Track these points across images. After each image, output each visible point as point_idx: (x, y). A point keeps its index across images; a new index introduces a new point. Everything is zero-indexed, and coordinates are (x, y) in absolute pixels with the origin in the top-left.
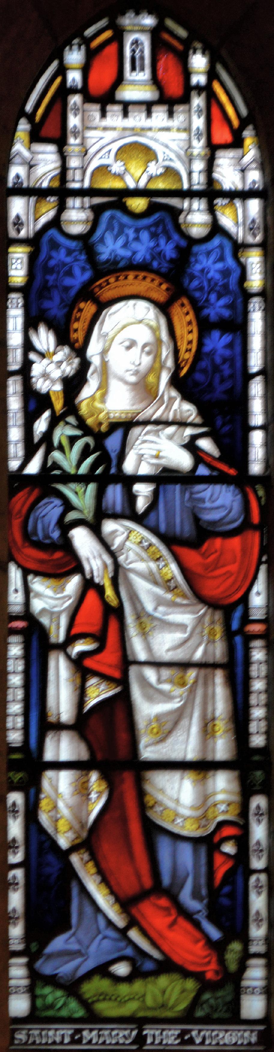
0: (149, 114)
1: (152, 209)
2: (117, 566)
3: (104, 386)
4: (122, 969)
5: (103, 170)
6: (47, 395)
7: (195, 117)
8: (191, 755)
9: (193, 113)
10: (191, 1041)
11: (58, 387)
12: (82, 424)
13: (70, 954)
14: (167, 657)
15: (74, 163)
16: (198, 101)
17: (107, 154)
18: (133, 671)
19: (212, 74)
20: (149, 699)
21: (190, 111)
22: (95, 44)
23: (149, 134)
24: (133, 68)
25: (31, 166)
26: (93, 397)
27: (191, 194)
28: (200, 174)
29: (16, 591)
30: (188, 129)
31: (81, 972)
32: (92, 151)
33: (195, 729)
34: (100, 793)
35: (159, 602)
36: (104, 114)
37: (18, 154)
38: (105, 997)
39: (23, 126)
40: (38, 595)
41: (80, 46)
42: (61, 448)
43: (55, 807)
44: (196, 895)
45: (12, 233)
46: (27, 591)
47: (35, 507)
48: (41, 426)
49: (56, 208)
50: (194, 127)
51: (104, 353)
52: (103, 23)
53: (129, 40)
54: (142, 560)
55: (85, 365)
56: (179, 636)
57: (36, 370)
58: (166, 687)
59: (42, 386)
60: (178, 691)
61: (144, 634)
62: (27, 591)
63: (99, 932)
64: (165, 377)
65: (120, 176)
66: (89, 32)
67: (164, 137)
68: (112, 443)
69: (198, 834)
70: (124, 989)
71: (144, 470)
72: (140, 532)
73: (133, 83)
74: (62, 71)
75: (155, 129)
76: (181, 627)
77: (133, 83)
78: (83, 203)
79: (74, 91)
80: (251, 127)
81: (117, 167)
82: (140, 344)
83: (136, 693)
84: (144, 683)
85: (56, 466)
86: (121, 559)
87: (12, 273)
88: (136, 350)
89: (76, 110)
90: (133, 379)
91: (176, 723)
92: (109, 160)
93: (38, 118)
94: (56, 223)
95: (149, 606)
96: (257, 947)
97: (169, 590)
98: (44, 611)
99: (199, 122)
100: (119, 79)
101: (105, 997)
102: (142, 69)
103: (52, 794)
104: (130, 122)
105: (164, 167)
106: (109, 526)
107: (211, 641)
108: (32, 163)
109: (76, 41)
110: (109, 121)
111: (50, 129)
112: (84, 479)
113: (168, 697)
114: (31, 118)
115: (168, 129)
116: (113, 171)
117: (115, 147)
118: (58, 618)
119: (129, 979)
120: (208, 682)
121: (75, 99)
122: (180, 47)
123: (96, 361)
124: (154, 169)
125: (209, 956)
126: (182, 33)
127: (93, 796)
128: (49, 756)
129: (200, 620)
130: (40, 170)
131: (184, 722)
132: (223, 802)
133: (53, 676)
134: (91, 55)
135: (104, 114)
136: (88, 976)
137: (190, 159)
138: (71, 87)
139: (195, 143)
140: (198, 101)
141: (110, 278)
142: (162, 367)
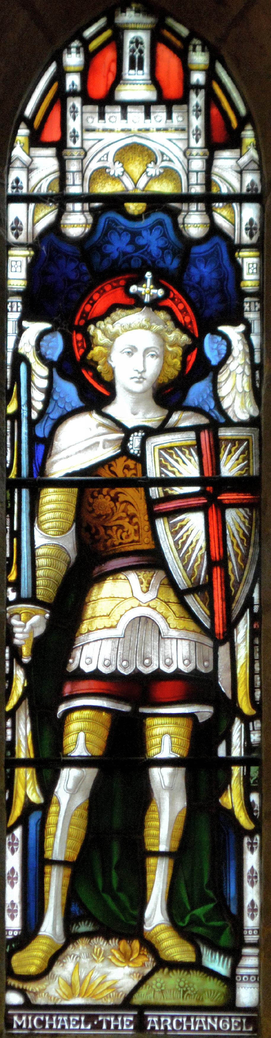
5: (102, 172)
7: (193, 118)
8: (37, 544)
9: (191, 114)
15: (73, 166)
16: (197, 100)
17: (106, 156)
19: (211, 74)
21: (188, 111)
22: (93, 45)
23: (148, 135)
24: (132, 67)
25: (29, 170)
28: (49, 412)
32: (90, 154)
36: (102, 116)
37: (18, 159)
39: (23, 132)
41: (78, 49)
45: (11, 237)
49: (57, 210)
50: (193, 127)
52: (102, 22)
53: (130, 36)
65: (118, 179)
66: (88, 33)
73: (133, 82)
74: (60, 75)
75: (153, 131)
78: (83, 207)
80: (249, 127)
81: (117, 169)
87: (10, 275)
88: (138, 355)
93: (37, 123)
96: (251, 938)
99: (197, 122)
100: (118, 79)
102: (141, 68)
105: (162, 167)
108: (31, 167)
109: (76, 44)
114: (29, 123)
115: (166, 130)
116: (112, 173)
121: (76, 102)
126: (184, 31)
133: (32, 794)
134: (89, 57)
135: (102, 116)
138: (70, 90)
139: (193, 143)
140: (197, 100)
141: (104, 286)
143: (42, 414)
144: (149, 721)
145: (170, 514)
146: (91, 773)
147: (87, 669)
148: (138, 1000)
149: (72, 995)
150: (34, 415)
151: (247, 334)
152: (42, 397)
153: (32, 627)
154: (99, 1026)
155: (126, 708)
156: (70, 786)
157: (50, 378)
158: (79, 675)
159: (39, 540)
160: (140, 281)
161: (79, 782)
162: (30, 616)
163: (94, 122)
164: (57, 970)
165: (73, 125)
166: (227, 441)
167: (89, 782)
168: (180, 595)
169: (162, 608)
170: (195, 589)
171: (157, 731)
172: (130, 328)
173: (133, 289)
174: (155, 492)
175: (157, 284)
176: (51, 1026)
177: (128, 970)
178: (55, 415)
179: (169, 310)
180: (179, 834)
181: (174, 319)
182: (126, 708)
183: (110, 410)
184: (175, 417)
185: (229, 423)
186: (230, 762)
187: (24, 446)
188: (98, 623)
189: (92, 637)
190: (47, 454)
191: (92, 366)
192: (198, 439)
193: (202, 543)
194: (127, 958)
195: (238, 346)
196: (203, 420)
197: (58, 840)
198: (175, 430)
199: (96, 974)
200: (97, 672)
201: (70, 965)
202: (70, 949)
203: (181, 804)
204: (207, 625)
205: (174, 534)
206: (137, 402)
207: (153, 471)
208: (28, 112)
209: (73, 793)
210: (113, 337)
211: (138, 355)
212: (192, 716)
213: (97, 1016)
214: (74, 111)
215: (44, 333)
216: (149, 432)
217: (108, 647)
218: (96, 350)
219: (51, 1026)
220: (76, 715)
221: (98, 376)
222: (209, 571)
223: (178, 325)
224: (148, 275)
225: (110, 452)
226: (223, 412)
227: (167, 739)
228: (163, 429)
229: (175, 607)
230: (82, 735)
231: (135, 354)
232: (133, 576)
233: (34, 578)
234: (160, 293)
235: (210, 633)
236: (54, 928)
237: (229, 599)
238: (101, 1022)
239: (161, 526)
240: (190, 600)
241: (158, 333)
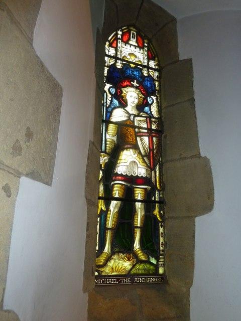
1: (136, 67)
5: (125, 56)
8: (107, 138)
27: (144, 66)
36: (126, 45)
39: (107, 43)
79: (119, 39)
81: (129, 57)
82: (133, 97)
88: (133, 98)
100: (129, 39)
111: (114, 45)
114: (109, 41)
124: (137, 60)
134: (123, 33)
135: (126, 45)
140: (146, 49)
143: (110, 106)
144: (135, 189)
145: (140, 136)
146: (119, 202)
147: (119, 173)
148: (132, 272)
149: (113, 272)
150: (108, 106)
151: (157, 99)
152: (109, 102)
153: (105, 160)
154: (120, 282)
155: (129, 185)
156: (114, 206)
157: (112, 98)
158: (117, 175)
159: (108, 137)
160: (134, 82)
161: (116, 205)
162: (104, 157)
163: (124, 46)
164: (109, 264)
165: (119, 45)
166: (153, 121)
167: (119, 205)
168: (143, 157)
169: (139, 159)
170: (145, 156)
171: (137, 192)
172: (131, 91)
173: (132, 83)
174: (137, 130)
175: (137, 83)
176: (106, 282)
177: (129, 263)
178: (113, 107)
179: (140, 90)
180: (143, 222)
181: (141, 91)
182: (129, 185)
183: (126, 108)
184: (141, 114)
185: (154, 118)
186: (155, 202)
187: (105, 113)
188: (122, 161)
189: (120, 165)
190: (111, 115)
191: (122, 97)
192: (147, 120)
193: (148, 144)
194: (129, 259)
195: (155, 101)
196: (148, 116)
197: (111, 216)
198: (141, 116)
199: (120, 265)
200: (122, 174)
201: (112, 262)
202: (113, 257)
203: (143, 213)
204: (149, 165)
205: (141, 141)
206: (133, 108)
207: (136, 124)
208: (110, 38)
209: (114, 208)
210: (127, 92)
211: (133, 98)
212: (145, 189)
213: (119, 283)
214: (119, 42)
215: (110, 88)
216: (135, 116)
217: (125, 167)
218: (123, 94)
219: (106, 282)
220: (116, 185)
221: (123, 100)
222: (150, 152)
223: (142, 93)
224: (135, 81)
225: (126, 119)
226: (152, 115)
227: (139, 195)
228: (138, 116)
229: (141, 160)
230: (117, 191)
231: (132, 97)
232: (131, 150)
233: (106, 147)
234: (138, 85)
235: (149, 167)
236: (108, 250)
237: (154, 159)
238: (121, 281)
239: (138, 139)
240: (145, 158)
241: (137, 94)
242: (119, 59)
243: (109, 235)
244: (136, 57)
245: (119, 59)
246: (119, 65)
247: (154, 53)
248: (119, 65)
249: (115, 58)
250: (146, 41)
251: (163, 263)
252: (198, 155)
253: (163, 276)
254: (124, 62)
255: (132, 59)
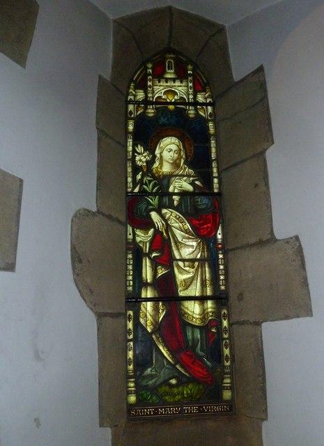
0: (174, 82)
2: (167, 224)
3: (161, 164)
4: (173, 381)
6: (141, 166)
10: (204, 411)
11: (145, 164)
12: (153, 176)
13: (151, 376)
14: (187, 257)
15: (150, 95)
18: (175, 263)
20: (181, 273)
25: (135, 96)
26: (157, 167)
27: (189, 104)
29: (130, 234)
30: (187, 86)
31: (158, 383)
33: (199, 284)
34: (163, 310)
35: (184, 237)
38: (167, 394)
40: (138, 236)
42: (146, 184)
43: (146, 316)
44: (202, 350)
46: (134, 234)
47: (152, 221)
48: (139, 177)
51: (161, 153)
54: (177, 222)
55: (154, 157)
56: (191, 250)
57: (137, 158)
58: (187, 269)
59: (139, 163)
60: (192, 270)
61: (178, 249)
62: (134, 234)
63: (164, 366)
64: (182, 161)
67: (180, 88)
68: (165, 182)
69: (201, 325)
70: (175, 390)
71: (176, 191)
72: (175, 213)
76: (192, 246)
77: (169, 73)
79: (150, 75)
83: (176, 270)
84: (178, 266)
85: (144, 189)
86: (169, 222)
89: (150, 80)
90: (172, 162)
91: (191, 283)
92: (162, 95)
94: (144, 113)
95: (180, 240)
97: (187, 233)
98: (140, 241)
101: (167, 394)
103: (145, 310)
104: (168, 84)
106: (164, 211)
107: (203, 251)
110: (161, 84)
112: (155, 195)
113: (188, 272)
117: (163, 91)
118: (146, 244)
119: (176, 386)
120: (202, 266)
122: (203, 85)
123: (158, 156)
125: (137, 328)
127: (161, 311)
128: (143, 296)
129: (199, 244)
130: (138, 97)
131: (195, 282)
132: (210, 312)
135: (159, 82)
136: (161, 385)
137: (189, 95)
140: (190, 78)
142: (182, 157)
219: (191, 411)
242: (152, 103)
243: (208, 282)
244: (175, 93)
245: (152, 103)
246: (151, 112)
247: (203, 81)
248: (151, 112)
249: (146, 102)
250: (190, 67)
251: (229, 385)
252: (100, 316)
253: (230, 404)
254: (158, 106)
255: (171, 98)
